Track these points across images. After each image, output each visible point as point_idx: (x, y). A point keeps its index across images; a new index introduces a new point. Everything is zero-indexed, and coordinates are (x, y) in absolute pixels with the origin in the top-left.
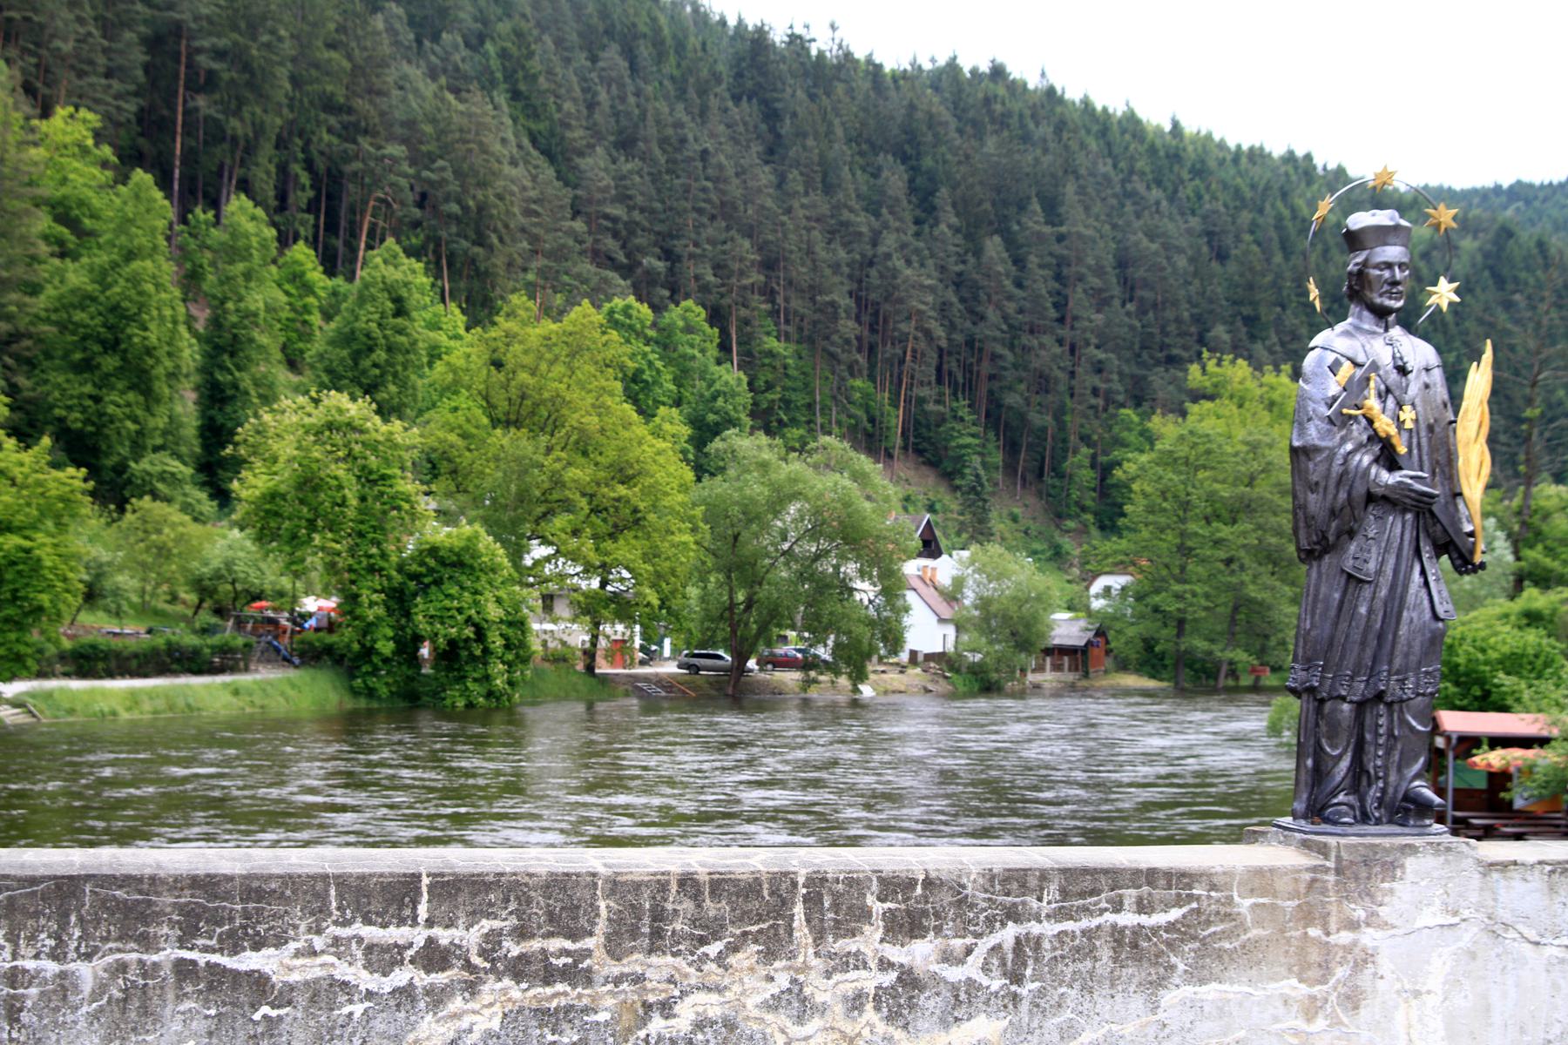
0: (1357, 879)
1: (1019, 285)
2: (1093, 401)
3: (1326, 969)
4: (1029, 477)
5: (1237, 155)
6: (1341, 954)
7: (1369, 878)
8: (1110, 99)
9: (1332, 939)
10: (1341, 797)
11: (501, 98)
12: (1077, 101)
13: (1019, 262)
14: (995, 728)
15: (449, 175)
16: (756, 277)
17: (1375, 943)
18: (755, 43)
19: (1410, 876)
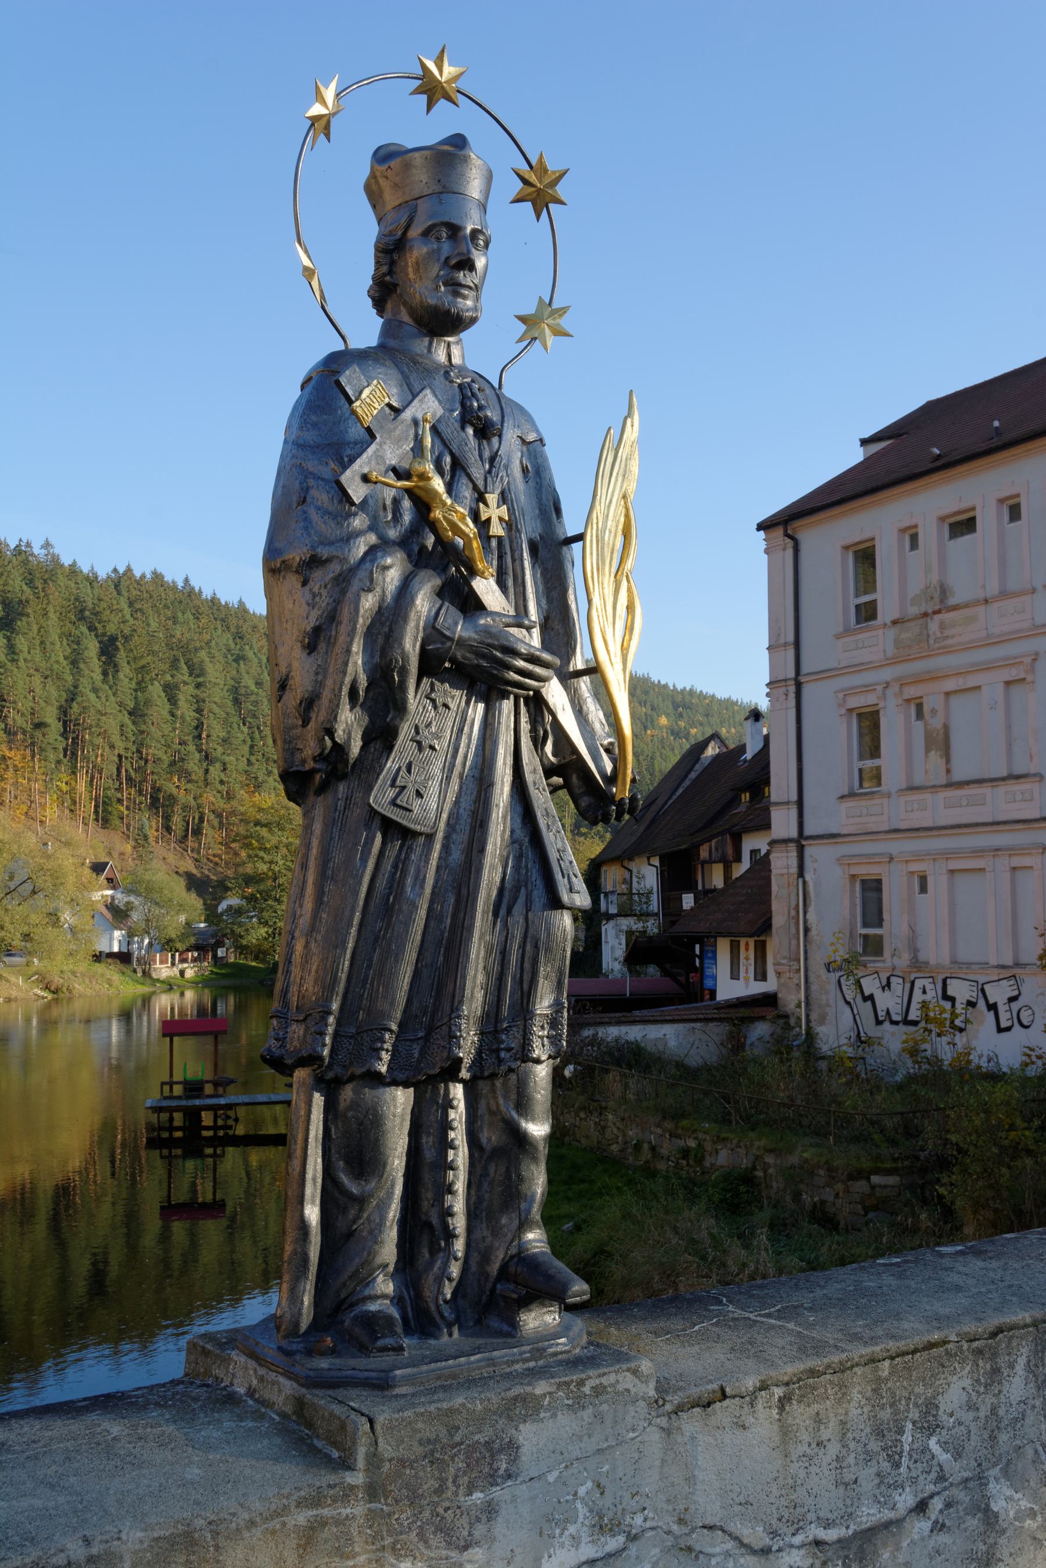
0: (414, 1498)
7: (439, 1491)
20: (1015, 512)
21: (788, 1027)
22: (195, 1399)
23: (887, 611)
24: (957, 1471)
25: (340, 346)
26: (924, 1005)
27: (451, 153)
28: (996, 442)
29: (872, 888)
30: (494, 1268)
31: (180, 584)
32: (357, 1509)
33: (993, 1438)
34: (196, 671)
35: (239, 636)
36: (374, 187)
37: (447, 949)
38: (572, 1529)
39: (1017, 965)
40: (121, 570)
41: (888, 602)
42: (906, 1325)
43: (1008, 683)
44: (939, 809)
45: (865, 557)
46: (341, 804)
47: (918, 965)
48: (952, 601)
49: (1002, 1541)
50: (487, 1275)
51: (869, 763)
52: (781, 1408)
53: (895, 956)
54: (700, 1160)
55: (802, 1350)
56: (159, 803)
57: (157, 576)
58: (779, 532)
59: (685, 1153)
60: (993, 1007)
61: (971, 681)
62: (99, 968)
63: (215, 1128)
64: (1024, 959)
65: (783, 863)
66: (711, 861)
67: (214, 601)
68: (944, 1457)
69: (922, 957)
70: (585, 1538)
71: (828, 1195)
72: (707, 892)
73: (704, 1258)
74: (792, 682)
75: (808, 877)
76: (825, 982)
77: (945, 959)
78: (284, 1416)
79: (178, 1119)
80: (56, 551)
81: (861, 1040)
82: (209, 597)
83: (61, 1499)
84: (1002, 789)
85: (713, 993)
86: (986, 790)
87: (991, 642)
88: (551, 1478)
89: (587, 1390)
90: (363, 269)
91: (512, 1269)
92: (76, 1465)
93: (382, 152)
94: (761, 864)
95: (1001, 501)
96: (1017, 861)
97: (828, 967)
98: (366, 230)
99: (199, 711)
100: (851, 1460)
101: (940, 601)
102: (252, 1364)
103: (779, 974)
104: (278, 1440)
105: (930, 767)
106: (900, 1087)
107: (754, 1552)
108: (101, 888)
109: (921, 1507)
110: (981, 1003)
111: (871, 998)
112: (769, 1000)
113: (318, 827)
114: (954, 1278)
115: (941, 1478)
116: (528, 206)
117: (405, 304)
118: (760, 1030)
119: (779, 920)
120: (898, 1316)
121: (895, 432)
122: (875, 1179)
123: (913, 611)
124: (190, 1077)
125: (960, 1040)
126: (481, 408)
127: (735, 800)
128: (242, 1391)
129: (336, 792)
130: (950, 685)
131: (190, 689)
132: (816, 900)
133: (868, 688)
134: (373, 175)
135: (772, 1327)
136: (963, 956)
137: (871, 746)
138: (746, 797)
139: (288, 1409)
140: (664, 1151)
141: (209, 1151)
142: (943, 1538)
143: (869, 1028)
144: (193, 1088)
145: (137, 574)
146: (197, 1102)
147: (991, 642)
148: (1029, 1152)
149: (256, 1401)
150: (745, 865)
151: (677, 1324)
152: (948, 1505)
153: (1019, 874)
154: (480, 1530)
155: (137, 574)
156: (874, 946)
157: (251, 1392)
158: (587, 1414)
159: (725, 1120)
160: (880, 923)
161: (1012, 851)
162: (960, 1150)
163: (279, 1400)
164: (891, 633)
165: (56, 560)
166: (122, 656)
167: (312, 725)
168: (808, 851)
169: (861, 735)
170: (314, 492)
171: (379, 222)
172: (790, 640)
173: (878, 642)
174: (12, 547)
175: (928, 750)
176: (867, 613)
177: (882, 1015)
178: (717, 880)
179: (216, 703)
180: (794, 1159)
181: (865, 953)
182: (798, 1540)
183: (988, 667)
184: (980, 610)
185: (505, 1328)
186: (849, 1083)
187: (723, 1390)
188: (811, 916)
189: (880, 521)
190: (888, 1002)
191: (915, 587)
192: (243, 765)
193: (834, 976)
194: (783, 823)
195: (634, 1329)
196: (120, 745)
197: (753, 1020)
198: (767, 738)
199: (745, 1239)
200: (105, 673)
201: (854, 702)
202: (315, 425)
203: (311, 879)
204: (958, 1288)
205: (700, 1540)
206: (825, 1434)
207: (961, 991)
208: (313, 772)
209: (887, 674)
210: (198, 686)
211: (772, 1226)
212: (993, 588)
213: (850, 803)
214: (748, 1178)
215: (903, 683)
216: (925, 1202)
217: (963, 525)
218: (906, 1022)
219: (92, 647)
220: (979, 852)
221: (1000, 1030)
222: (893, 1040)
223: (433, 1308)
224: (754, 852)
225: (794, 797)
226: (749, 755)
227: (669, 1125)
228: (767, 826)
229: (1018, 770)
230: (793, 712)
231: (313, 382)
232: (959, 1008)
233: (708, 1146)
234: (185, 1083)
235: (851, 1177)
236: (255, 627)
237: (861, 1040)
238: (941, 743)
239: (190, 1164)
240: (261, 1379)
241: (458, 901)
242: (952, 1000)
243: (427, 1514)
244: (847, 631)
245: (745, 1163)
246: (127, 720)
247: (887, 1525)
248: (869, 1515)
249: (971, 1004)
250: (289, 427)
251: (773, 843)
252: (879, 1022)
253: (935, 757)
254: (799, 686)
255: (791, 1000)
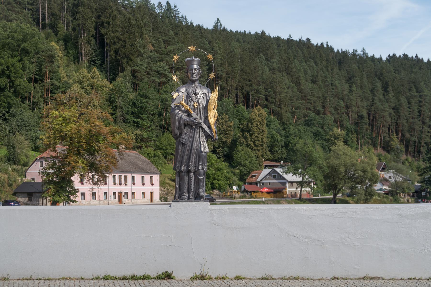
1: (409, 107)
2: (428, 134)
4: (411, 153)
8: (241, 30)
11: (285, 74)
12: (315, 45)
13: (409, 103)
14: (186, 156)
15: (272, 93)
16: (344, 110)
18: (345, 54)
57: (405, 56)
80: (366, 52)
82: (426, 61)
145: (398, 56)
165: (366, 55)
166: (390, 88)
174: (351, 53)
179: (427, 102)
219: (379, 85)
246: (392, 111)
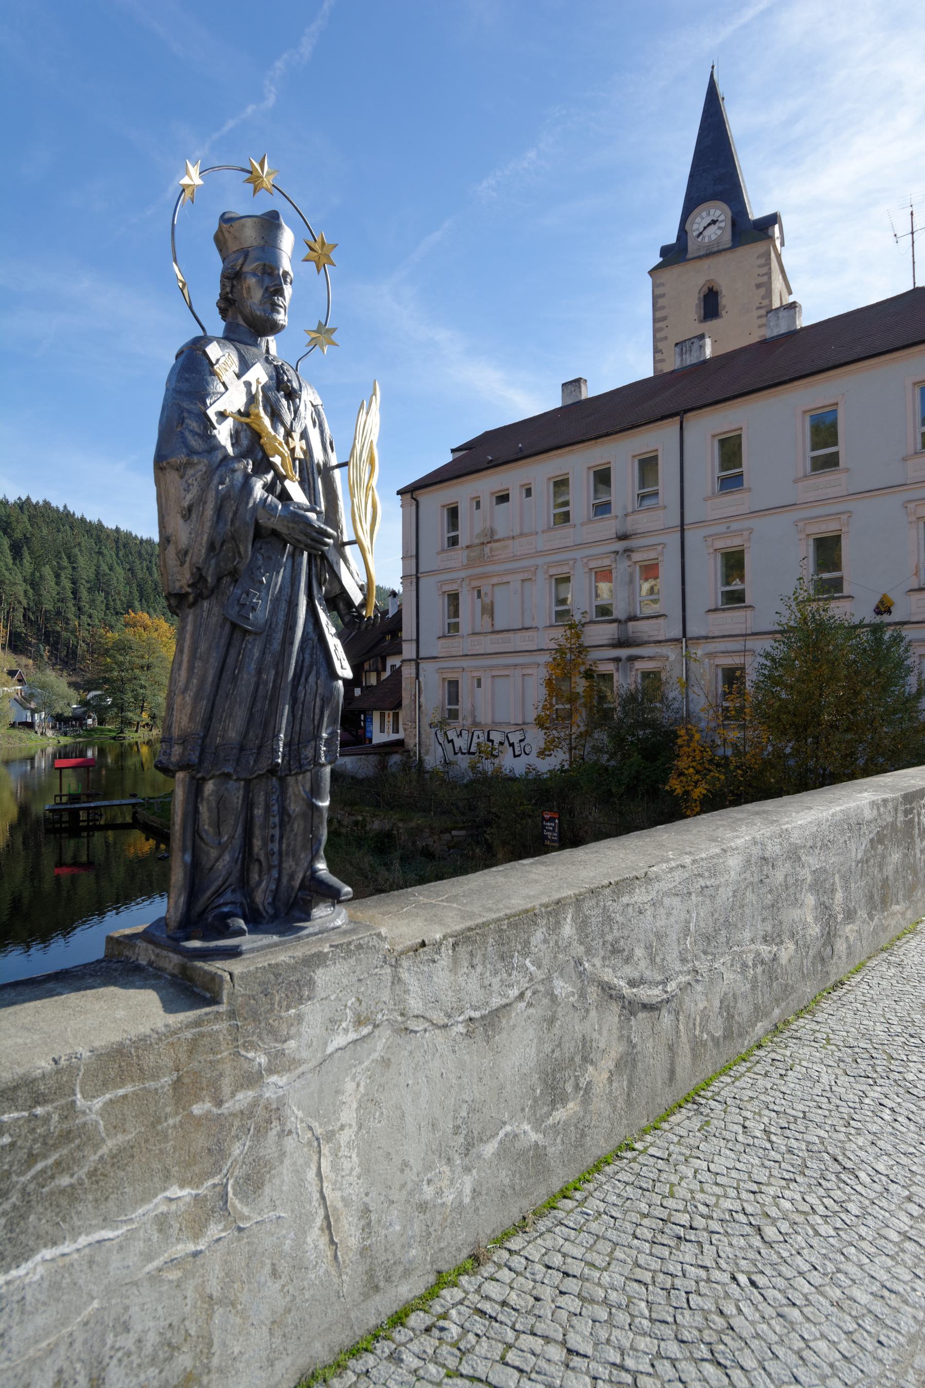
3: (218, 1153)
5: (142, 541)
6: (237, 1123)
9: (228, 1106)
10: (228, 897)
17: (281, 1092)
19: (320, 993)
20: (529, 492)
21: (409, 757)
22: (115, 970)
23: (463, 541)
24: (540, 975)
25: (201, 334)
26: (478, 744)
27: (270, 224)
28: (520, 455)
29: (454, 685)
30: (297, 883)
31: (61, 509)
32: (222, 1026)
33: (555, 957)
34: (71, 559)
35: (98, 541)
36: (221, 238)
37: (270, 701)
38: (344, 1025)
39: (524, 723)
40: (24, 499)
41: (465, 535)
42: (513, 901)
43: (523, 581)
44: (488, 644)
45: (453, 513)
46: (205, 615)
47: (475, 724)
48: (496, 537)
49: (559, 1009)
50: (293, 888)
51: (453, 620)
52: (454, 950)
53: (464, 720)
54: (364, 827)
55: (463, 917)
56: (51, 638)
57: (47, 504)
58: (409, 496)
59: (356, 823)
60: (512, 745)
61: (505, 579)
62: (15, 732)
63: (88, 821)
64: (528, 721)
65: (408, 672)
66: (370, 671)
67: (83, 520)
68: (533, 968)
69: (478, 720)
70: (351, 1029)
71: (430, 841)
72: (368, 687)
73: (366, 877)
74: (414, 576)
75: (421, 679)
76: (429, 735)
77: (489, 721)
78: (173, 975)
79: (66, 818)
81: (447, 763)
83: (36, 1037)
84: (520, 634)
85: (371, 740)
86: (511, 635)
87: (515, 559)
88: (332, 998)
89: (352, 947)
90: (214, 293)
91: (307, 883)
92: (43, 1016)
93: (227, 216)
94: (397, 673)
95: (522, 486)
96: (525, 671)
97: (431, 725)
98: (216, 265)
99: (74, 583)
100: (488, 974)
101: (490, 537)
102: (151, 947)
103: (405, 730)
104: (172, 990)
105: (483, 623)
106: (466, 786)
107: (439, 1027)
108: (14, 685)
109: (522, 995)
110: (506, 743)
111: (452, 741)
112: (400, 743)
113: (189, 628)
114: (533, 876)
115: (531, 980)
116: (313, 265)
117: (241, 313)
118: (396, 758)
119: (405, 702)
120: (509, 897)
121: (468, 447)
122: (454, 833)
123: (477, 541)
124: (72, 792)
125: (497, 761)
126: (289, 380)
127: (383, 639)
128: (144, 963)
129: (202, 606)
130: (495, 580)
131: (70, 571)
132: (425, 691)
133: (453, 581)
134: (220, 229)
135: (444, 907)
136: (497, 720)
137: (454, 610)
138: (388, 637)
139: (176, 971)
140: (345, 823)
141: (85, 834)
142: (531, 1011)
143: (451, 756)
144: (74, 798)
145: (34, 501)
146: (77, 806)
147: (515, 559)
148: (530, 816)
149: (155, 968)
150: (388, 673)
151: (393, 908)
152: (534, 993)
153: (526, 678)
154: (293, 1030)
155: (34, 501)
156: (454, 714)
157: (150, 963)
158: (352, 961)
159: (377, 805)
160: (457, 703)
161: (523, 666)
162: (497, 816)
163: (169, 967)
164: (466, 552)
167: (187, 565)
168: (421, 666)
169: (449, 605)
170: (187, 421)
171: (224, 260)
172: (413, 554)
173: (459, 556)
175: (483, 614)
176: (454, 541)
177: (457, 749)
178: (373, 680)
180: (413, 824)
181: (449, 718)
182: (461, 1019)
183: (513, 572)
184: (510, 542)
185: (303, 916)
186: (441, 785)
187: (423, 942)
188: (422, 700)
189: (460, 493)
190: (460, 743)
191: (478, 529)
192: (102, 615)
193: (433, 730)
194: (408, 651)
195: (370, 913)
196: (25, 602)
197: (391, 753)
198: (400, 605)
199: (388, 866)
200: (14, 559)
201: (445, 588)
202: (187, 380)
203: (185, 658)
204: (536, 881)
205: (413, 1025)
206: (475, 962)
207: (496, 737)
208: (187, 594)
209: (463, 574)
210: (74, 568)
211: (401, 859)
212: (517, 531)
213: (443, 641)
214: (389, 835)
215: (471, 578)
216: (478, 843)
217: (503, 498)
218: (469, 753)
220: (507, 666)
221: (515, 756)
222: (464, 762)
223: (261, 908)
224: (393, 666)
225: (414, 637)
226: (390, 615)
227: (348, 809)
228: (400, 652)
229: (526, 626)
230: (414, 593)
231: (183, 356)
232: (496, 745)
233: (368, 819)
234: (69, 795)
235: (442, 832)
236: (108, 536)
237: (447, 763)
238: (489, 610)
239: (72, 842)
240: (157, 955)
241: (277, 673)
242: (492, 741)
243: (263, 1024)
244: (443, 550)
245: (388, 827)
247: (505, 1006)
248: (496, 1002)
249: (501, 744)
250: (169, 380)
251: (403, 661)
252: (456, 754)
253: (486, 618)
254: (418, 579)
255: (411, 742)
